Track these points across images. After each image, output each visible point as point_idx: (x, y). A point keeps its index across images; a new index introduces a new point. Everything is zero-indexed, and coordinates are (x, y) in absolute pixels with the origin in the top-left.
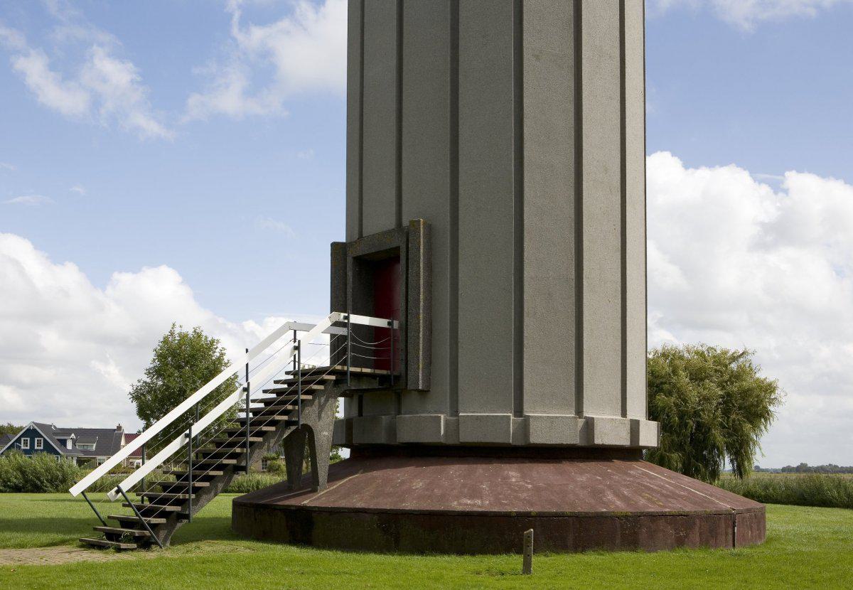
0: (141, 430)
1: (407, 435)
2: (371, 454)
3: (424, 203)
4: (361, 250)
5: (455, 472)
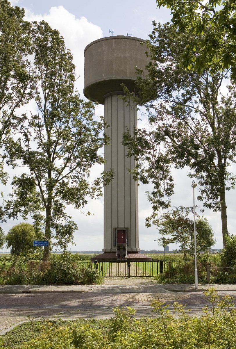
4: (118, 229)
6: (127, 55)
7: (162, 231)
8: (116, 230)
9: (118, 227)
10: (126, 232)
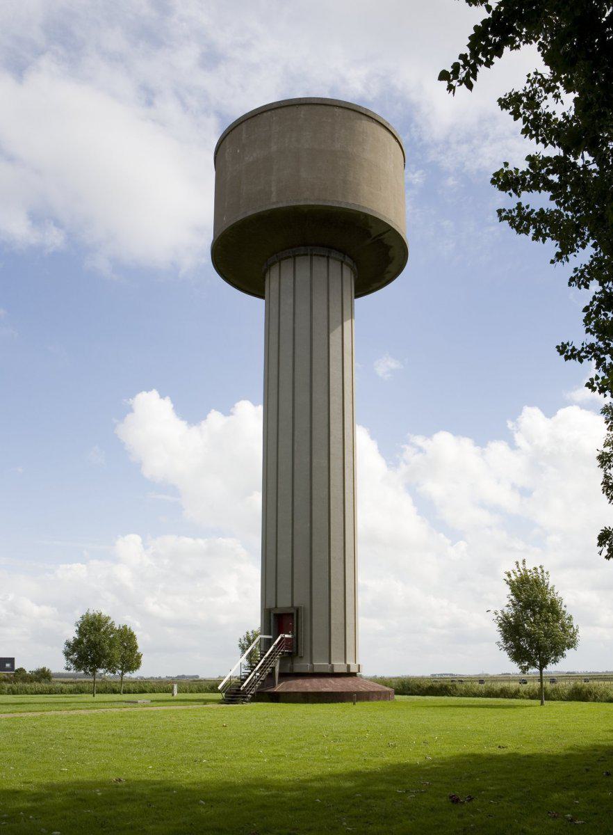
0: (137, 691)
1: (297, 670)
2: (284, 676)
5: (315, 681)
6: (274, 148)
8: (272, 614)
9: (276, 607)
10: (295, 618)
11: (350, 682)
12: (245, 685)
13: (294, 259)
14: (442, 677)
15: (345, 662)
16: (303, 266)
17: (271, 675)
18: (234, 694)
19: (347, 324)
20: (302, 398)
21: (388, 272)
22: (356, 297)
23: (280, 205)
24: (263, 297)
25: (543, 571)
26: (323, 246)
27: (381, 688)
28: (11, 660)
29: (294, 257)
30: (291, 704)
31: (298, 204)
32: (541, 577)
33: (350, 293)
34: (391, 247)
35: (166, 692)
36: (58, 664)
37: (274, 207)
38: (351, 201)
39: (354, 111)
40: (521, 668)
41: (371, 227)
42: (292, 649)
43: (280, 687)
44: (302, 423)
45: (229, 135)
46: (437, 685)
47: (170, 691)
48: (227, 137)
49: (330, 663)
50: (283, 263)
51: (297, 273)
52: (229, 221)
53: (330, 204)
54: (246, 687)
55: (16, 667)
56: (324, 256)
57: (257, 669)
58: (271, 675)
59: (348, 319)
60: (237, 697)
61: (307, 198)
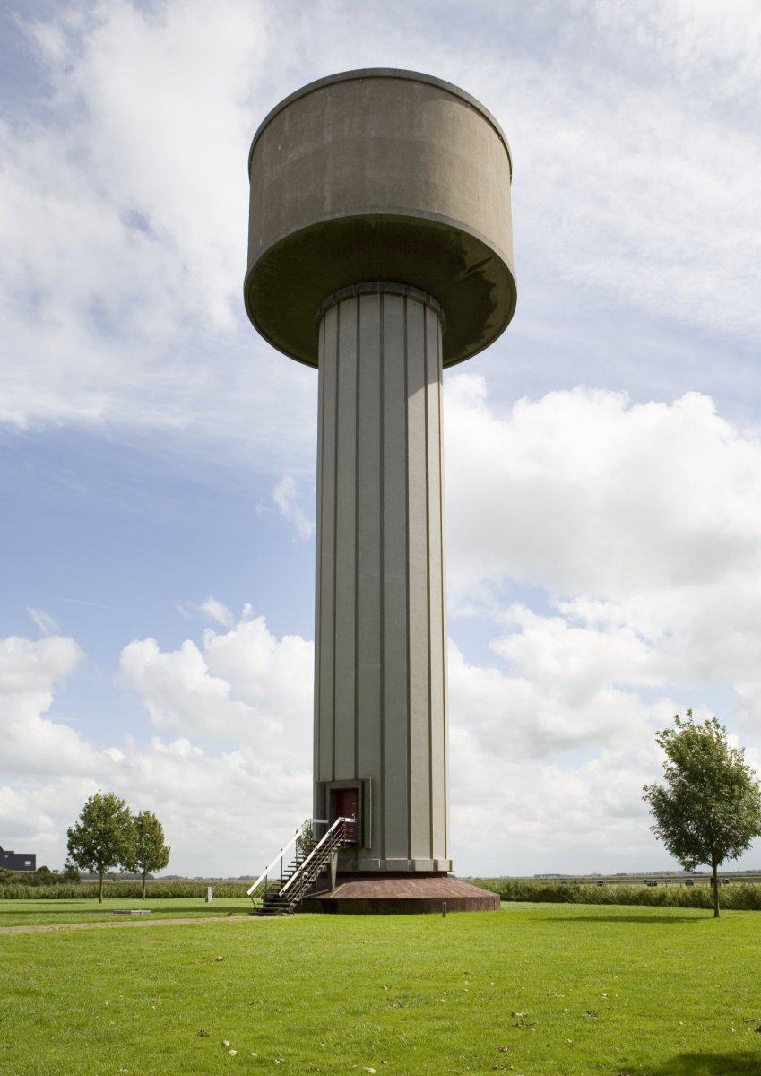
1: (363, 867)
2: (344, 876)
3: (368, 770)
4: (335, 786)
5: (388, 883)
6: (328, 138)
7: (222, 630)
8: (328, 792)
9: (334, 780)
10: (360, 794)
11: (438, 885)
12: (285, 888)
13: (359, 299)
14: (546, 878)
15: (432, 857)
16: (370, 306)
17: (325, 875)
18: (274, 902)
19: (432, 387)
20: (370, 489)
21: (490, 326)
22: (445, 366)
23: (337, 216)
24: (315, 365)
25: (718, 726)
26: (397, 281)
27: (477, 892)
28: (32, 858)
29: (358, 296)
30: (354, 916)
31: (361, 213)
32: (715, 736)
33: (436, 339)
34: (494, 285)
35: (12, 898)
36: (54, 855)
37: (328, 218)
38: (436, 211)
39: (442, 89)
40: (683, 864)
41: (465, 252)
42: (356, 838)
43: (339, 892)
44: (370, 524)
45: (268, 129)
46: (554, 886)
47: (204, 895)
48: (266, 132)
49: (409, 857)
50: (343, 305)
51: (362, 312)
52: (267, 244)
53: (406, 213)
54: (287, 891)
55: (38, 865)
56: (399, 295)
57: (303, 866)
58: (325, 875)
59: (434, 382)
60: (275, 906)
61: (374, 205)
